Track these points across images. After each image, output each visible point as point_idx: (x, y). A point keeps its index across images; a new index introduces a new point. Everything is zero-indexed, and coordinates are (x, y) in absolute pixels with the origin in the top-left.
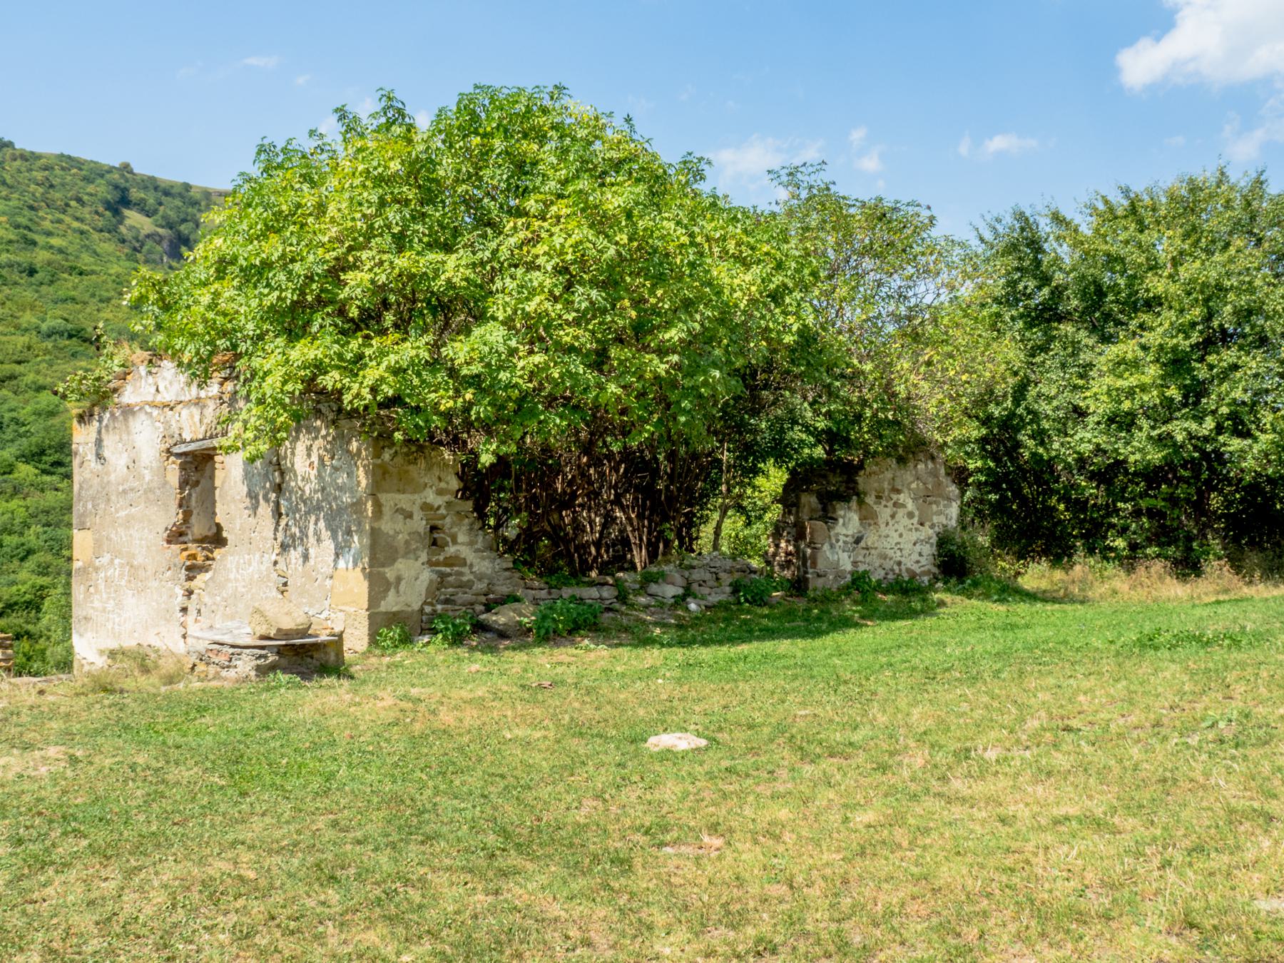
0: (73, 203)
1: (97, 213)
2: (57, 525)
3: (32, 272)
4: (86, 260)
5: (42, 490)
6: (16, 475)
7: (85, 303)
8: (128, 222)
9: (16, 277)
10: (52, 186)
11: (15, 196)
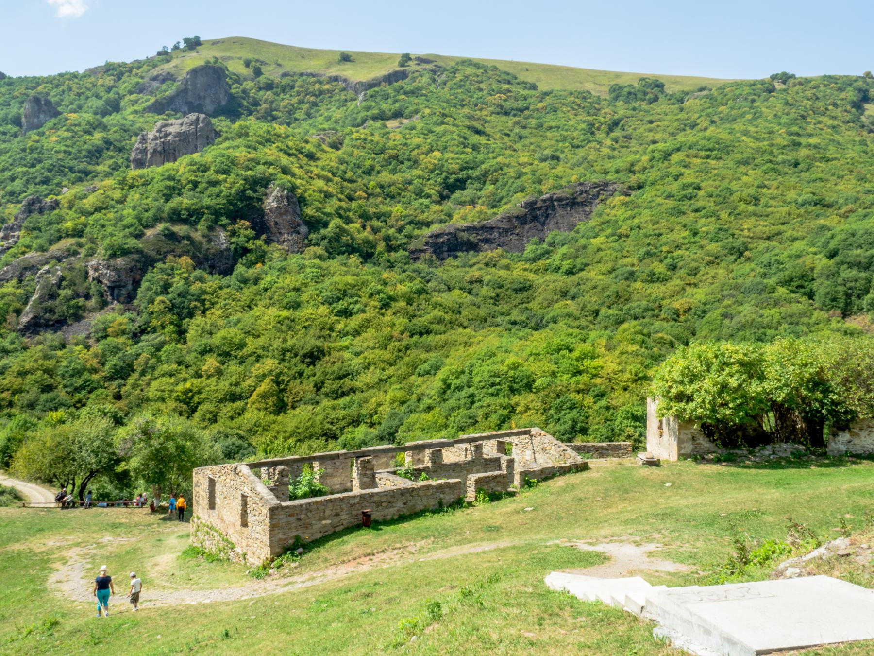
0: (830, 107)
1: (846, 111)
2: (797, 324)
3: (796, 164)
4: (832, 152)
5: (790, 303)
6: (776, 294)
7: (827, 180)
8: (867, 113)
9: (786, 170)
10: (817, 98)
11: (793, 111)
